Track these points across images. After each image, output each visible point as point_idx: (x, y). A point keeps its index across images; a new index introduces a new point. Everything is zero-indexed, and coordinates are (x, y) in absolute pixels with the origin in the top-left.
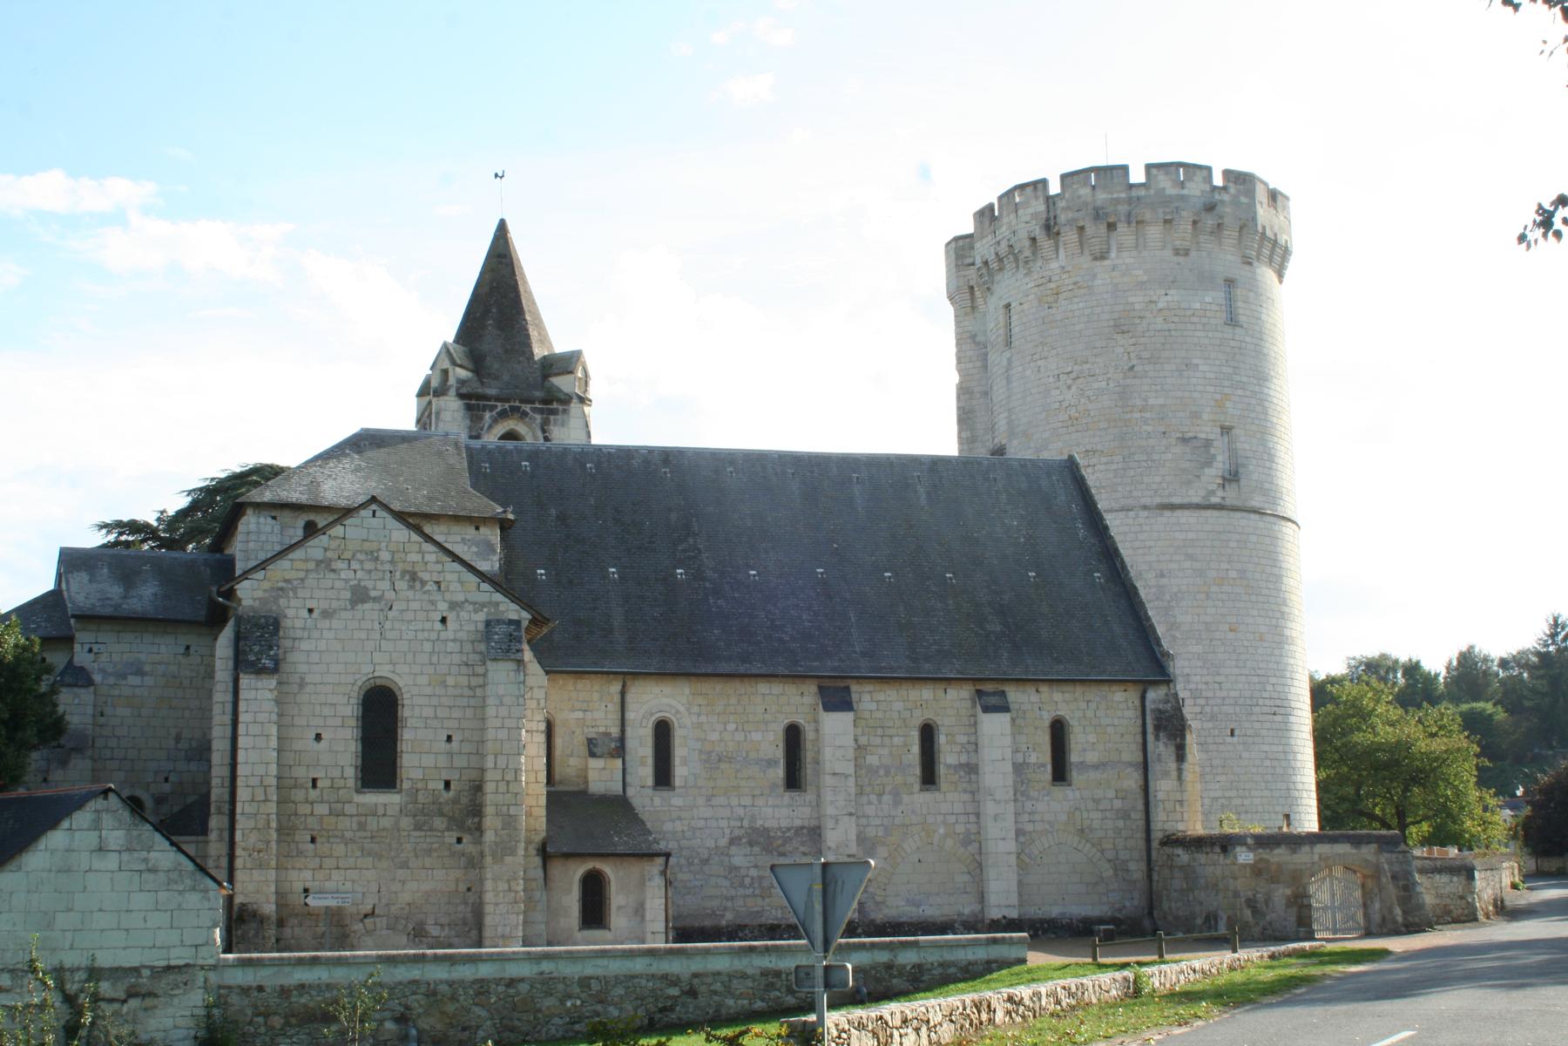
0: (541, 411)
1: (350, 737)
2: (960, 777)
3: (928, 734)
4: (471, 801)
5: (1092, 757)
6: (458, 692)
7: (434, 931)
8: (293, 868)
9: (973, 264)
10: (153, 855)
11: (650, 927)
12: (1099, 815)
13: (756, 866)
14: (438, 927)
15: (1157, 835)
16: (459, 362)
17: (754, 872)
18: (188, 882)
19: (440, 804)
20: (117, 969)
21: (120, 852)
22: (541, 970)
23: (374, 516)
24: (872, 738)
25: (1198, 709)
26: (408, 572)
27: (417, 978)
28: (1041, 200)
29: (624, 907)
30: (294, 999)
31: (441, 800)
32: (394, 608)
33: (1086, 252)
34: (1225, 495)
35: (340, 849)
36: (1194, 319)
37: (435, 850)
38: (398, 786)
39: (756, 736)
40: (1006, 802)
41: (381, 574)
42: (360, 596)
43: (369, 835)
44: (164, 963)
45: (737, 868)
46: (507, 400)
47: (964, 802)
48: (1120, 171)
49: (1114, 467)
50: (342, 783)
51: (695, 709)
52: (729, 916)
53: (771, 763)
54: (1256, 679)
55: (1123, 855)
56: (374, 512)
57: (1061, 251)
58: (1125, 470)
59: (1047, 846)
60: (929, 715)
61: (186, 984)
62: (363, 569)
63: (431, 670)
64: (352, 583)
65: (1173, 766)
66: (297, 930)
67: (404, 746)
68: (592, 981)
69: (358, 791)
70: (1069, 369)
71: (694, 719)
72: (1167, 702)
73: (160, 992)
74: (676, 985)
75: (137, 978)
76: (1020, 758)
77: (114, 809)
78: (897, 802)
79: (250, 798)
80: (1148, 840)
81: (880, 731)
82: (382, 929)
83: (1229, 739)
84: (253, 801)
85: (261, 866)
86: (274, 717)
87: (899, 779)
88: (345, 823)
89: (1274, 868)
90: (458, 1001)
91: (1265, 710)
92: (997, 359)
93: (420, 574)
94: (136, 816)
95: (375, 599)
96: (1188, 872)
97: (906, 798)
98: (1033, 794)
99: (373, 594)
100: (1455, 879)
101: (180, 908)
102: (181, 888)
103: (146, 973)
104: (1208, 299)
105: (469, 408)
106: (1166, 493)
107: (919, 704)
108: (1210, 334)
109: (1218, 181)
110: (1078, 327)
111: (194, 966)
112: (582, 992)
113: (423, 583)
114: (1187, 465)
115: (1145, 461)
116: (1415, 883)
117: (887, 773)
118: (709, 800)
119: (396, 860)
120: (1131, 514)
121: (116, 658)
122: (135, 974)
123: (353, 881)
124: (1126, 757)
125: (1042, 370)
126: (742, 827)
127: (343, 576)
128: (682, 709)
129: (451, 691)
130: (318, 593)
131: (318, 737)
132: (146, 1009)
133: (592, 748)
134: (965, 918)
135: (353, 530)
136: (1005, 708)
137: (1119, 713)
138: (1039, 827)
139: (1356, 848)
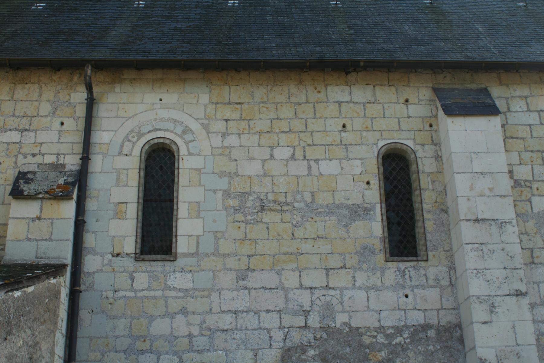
51: (220, 126)
71: (217, 141)
126: (306, 327)
128: (194, 126)
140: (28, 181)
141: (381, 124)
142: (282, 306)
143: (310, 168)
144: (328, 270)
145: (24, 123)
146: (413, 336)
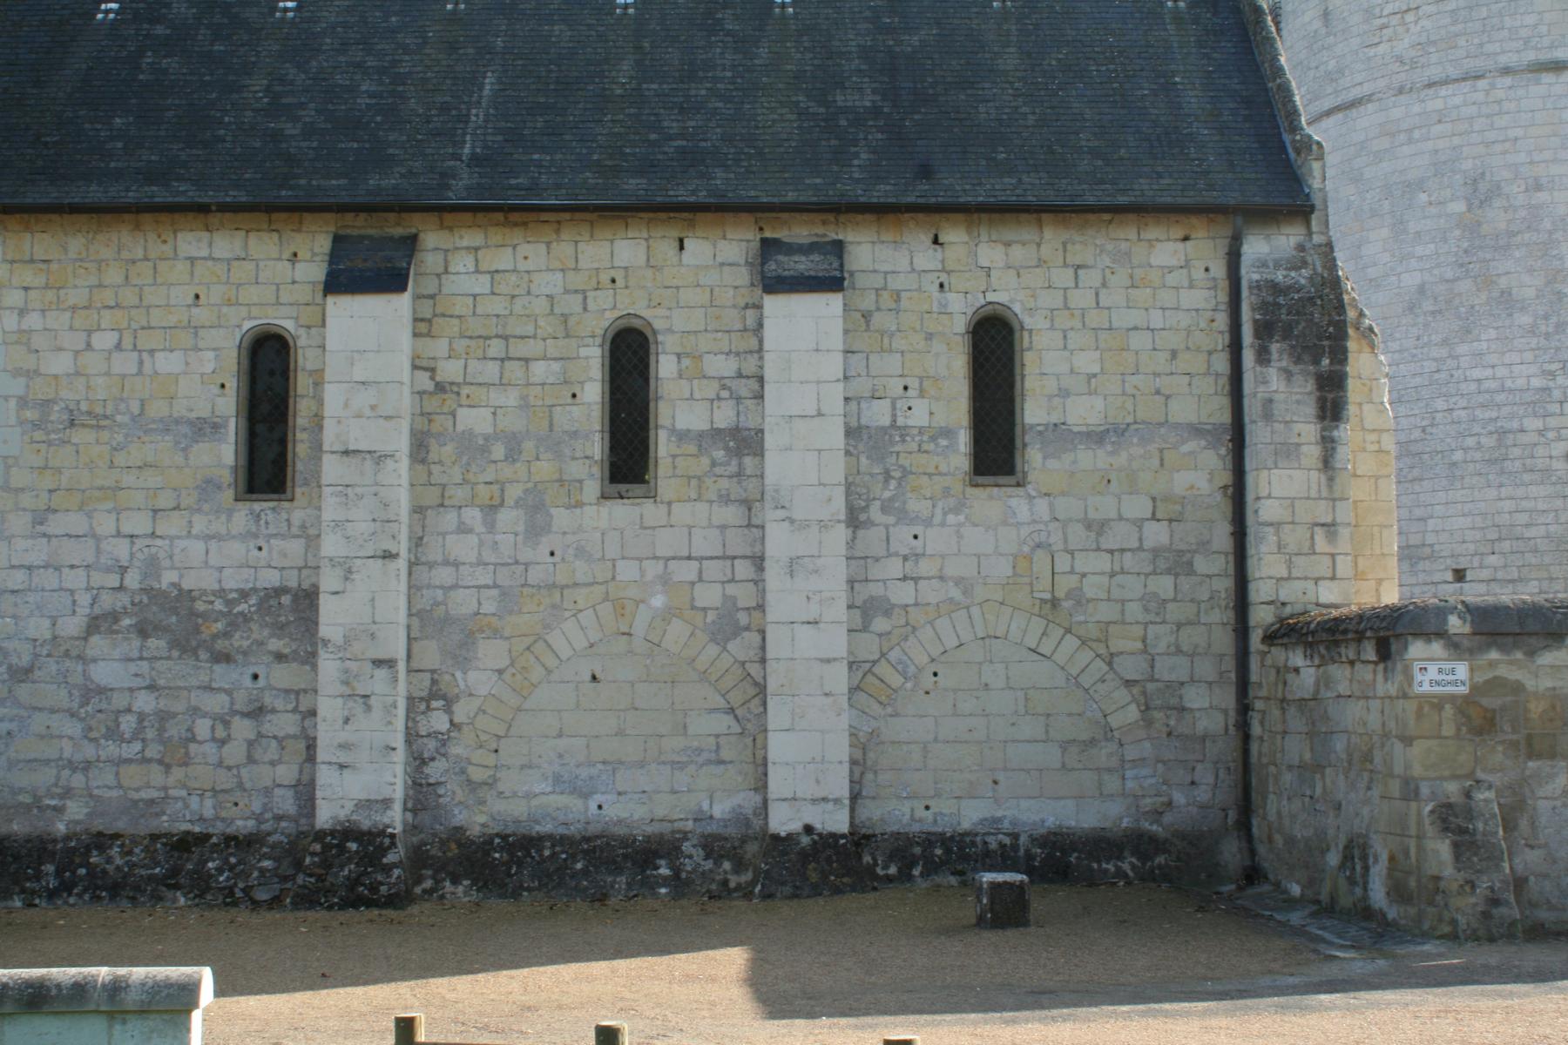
2: (714, 464)
5: (1085, 412)
12: (1103, 563)
13: (152, 687)
15: (1261, 617)
39: (168, 363)
45: (102, 691)
47: (723, 528)
52: (76, 811)
53: (204, 428)
65: (1308, 431)
76: (878, 414)
78: (536, 529)
81: (496, 348)
87: (545, 469)
97: (561, 517)
98: (915, 505)
106: (1546, 42)
107: (605, 278)
117: (512, 457)
120: (1482, 84)
124: (1184, 411)
126: (121, 588)
136: (832, 283)
137: (1166, 297)
138: (931, 593)
142: (90, 560)
143: (141, 363)
144: (155, 511)
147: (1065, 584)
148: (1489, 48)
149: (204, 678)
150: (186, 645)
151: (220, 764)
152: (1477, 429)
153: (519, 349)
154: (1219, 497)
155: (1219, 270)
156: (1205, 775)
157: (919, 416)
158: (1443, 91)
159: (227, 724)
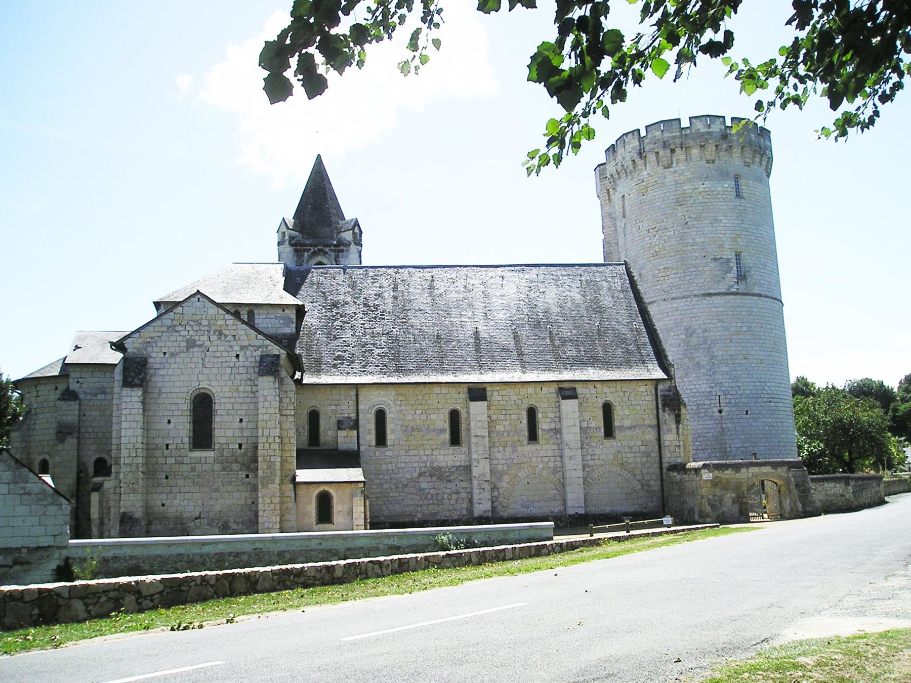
0: (334, 251)
1: (186, 421)
2: (551, 436)
3: (532, 413)
4: (253, 454)
5: (627, 423)
6: (246, 395)
7: (234, 526)
8: (156, 493)
9: (606, 177)
10: (28, 485)
11: (355, 522)
12: (632, 455)
13: (434, 488)
14: (236, 524)
15: (665, 465)
16: (291, 227)
17: (432, 491)
18: (50, 500)
19: (236, 456)
20: (7, 549)
21: (8, 484)
22: (255, 547)
23: (199, 301)
24: (499, 416)
25: (728, 401)
26: (217, 330)
27: (182, 552)
28: (637, 140)
29: (341, 511)
30: (110, 565)
31: (237, 454)
32: (210, 350)
33: (660, 165)
34: (738, 287)
35: (181, 482)
36: (719, 196)
37: (234, 482)
38: (213, 447)
39: (433, 417)
40: (577, 449)
41: (202, 332)
42: (191, 344)
43: (197, 474)
44: (36, 545)
45: (423, 489)
46: (316, 246)
47: (553, 450)
48: (676, 122)
49: (679, 275)
50: (182, 446)
51: (398, 403)
52: (419, 515)
53: (442, 431)
54: (758, 384)
55: (647, 477)
56: (199, 299)
57: (648, 165)
58: (684, 277)
59: (602, 473)
60: (532, 402)
61: (48, 557)
62: (193, 330)
63: (230, 383)
64: (187, 337)
65: (674, 426)
66: (158, 526)
67: (216, 425)
68: (286, 553)
69: (191, 450)
70: (654, 226)
71: (398, 408)
72: (669, 390)
73: (33, 562)
74: (336, 555)
75: (19, 553)
76: (585, 424)
77: (5, 460)
78: (514, 451)
79: (128, 455)
80: (661, 468)
81: (504, 412)
82: (204, 525)
83: (745, 416)
84: (129, 457)
85: (134, 491)
86: (141, 411)
87: (515, 438)
88: (184, 468)
89: (724, 481)
90: (206, 565)
91: (765, 400)
92: (620, 224)
93: (224, 332)
94: (19, 464)
95: (200, 346)
96: (680, 483)
97: (519, 448)
98: (593, 444)
99: (198, 343)
100: (838, 485)
101: (44, 514)
102: (45, 503)
103: (24, 551)
104: (725, 186)
105: (296, 251)
106: (707, 287)
107: (526, 396)
108: (728, 204)
109: (728, 123)
110: (658, 204)
111: (53, 546)
112: (280, 560)
113: (226, 336)
114: (717, 272)
115: (695, 271)
116: (809, 489)
117: (508, 435)
118: (406, 452)
119: (212, 488)
120: (689, 299)
121: (91, 385)
122: (18, 551)
123: (188, 499)
124: (647, 422)
125: (641, 227)
126: (426, 466)
127: (182, 333)
128: (391, 403)
129: (242, 395)
130: (168, 344)
131: (169, 422)
132: (25, 571)
133: (340, 425)
134: (555, 514)
135: (188, 310)
136: (575, 397)
137: (643, 398)
138: (597, 462)
139: (774, 469)
140: (342, 424)
141: (450, 401)
142: (419, 460)
143: (427, 417)
144: (432, 449)
145: (336, 403)
146: (456, 469)
147: (625, 460)
148: (690, 289)
149: (445, 485)
150: (441, 478)
151: (450, 504)
152: (691, 404)
153: (509, 412)
154: (655, 440)
155: (653, 392)
156: (655, 499)
157: (593, 425)
158: (677, 301)
159: (451, 496)
